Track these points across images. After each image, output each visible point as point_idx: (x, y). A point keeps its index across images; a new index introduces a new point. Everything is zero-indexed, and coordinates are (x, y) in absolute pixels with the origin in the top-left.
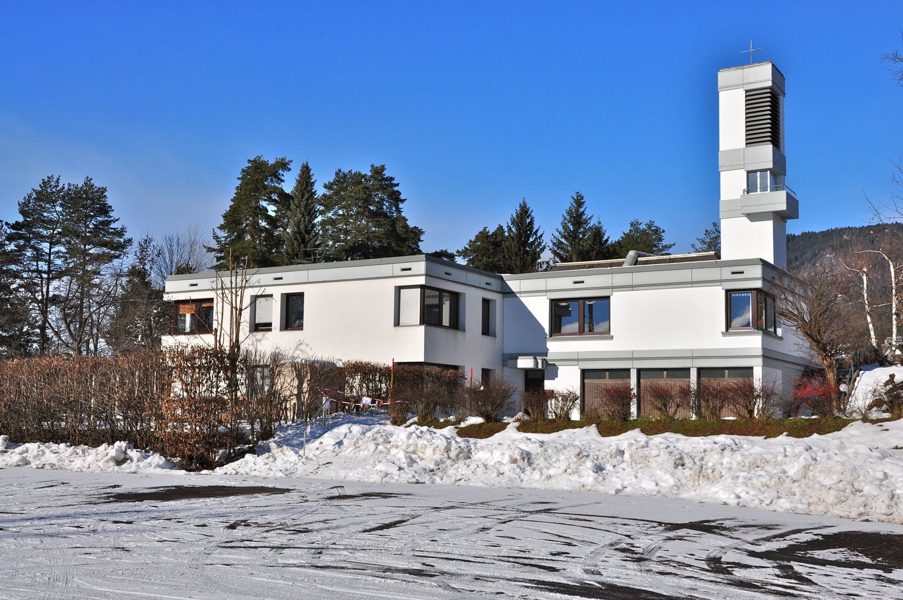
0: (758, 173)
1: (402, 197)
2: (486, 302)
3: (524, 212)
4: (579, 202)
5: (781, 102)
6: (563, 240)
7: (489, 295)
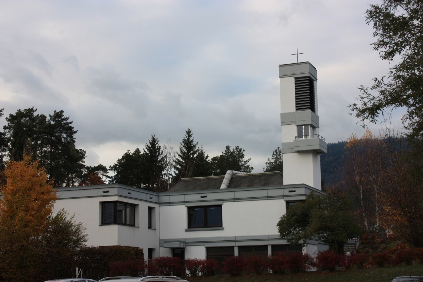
0: (303, 127)
1: (75, 130)
2: (150, 209)
3: (154, 142)
4: (189, 134)
5: (315, 85)
6: (181, 160)
7: (152, 205)
